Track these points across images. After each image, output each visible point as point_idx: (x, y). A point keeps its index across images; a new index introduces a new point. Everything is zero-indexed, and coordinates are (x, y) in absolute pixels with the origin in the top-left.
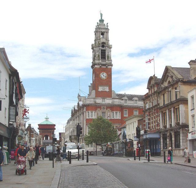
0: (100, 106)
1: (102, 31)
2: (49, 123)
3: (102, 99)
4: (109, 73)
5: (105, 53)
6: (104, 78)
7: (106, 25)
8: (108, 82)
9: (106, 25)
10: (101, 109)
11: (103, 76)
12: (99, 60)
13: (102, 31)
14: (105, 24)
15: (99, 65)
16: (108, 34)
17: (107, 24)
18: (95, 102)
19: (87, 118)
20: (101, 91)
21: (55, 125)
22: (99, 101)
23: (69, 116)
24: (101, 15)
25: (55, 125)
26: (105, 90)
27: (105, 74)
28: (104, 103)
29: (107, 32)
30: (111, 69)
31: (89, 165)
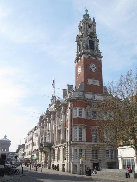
0: (90, 103)
1: (88, 26)
2: (6, 140)
3: (92, 94)
4: (99, 66)
5: (93, 44)
6: (94, 71)
7: (92, 20)
8: (98, 75)
9: (92, 20)
10: (91, 107)
11: (93, 67)
12: (88, 50)
13: (88, 26)
14: (91, 19)
15: (88, 54)
16: (95, 27)
17: (94, 18)
18: (85, 97)
19: (74, 117)
20: (91, 84)
21: (10, 141)
22: (89, 96)
23: (36, 122)
24: (87, 11)
25: (10, 141)
26: (96, 84)
27: (94, 66)
28: (94, 99)
29: (94, 26)
30: (101, 61)
31: (24, 176)
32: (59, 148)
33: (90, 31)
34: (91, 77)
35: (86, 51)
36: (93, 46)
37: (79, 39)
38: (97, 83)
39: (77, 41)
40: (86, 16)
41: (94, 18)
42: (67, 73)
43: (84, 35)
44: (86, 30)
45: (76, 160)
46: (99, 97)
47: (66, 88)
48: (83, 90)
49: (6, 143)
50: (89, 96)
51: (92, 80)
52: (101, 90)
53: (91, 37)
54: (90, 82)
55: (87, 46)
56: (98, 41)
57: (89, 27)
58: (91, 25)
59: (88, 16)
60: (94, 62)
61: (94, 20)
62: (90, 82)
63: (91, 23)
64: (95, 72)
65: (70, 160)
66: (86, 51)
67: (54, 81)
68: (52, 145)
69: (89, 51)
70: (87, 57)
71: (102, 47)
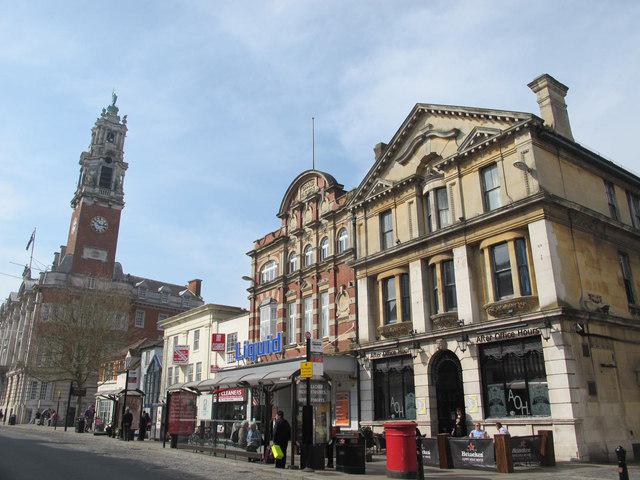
1: (110, 132)
5: (110, 175)
11: (100, 224)
13: (110, 132)
17: (125, 117)
24: (115, 98)
27: (102, 221)
29: (123, 134)
32: (611, 366)
33: (109, 146)
34: (92, 244)
35: (91, 190)
36: (110, 180)
37: (85, 159)
38: (103, 256)
39: (81, 163)
40: (114, 109)
41: (125, 117)
42: (58, 229)
43: (94, 154)
44: (102, 144)
45: (32, 402)
46: (102, 285)
47: (59, 251)
48: (69, 268)
49: (95, 306)
50: (78, 281)
51: (91, 250)
52: (111, 269)
53: (108, 160)
54: (88, 253)
55: (94, 180)
56: (125, 166)
57: (111, 135)
58: (116, 132)
59: (116, 110)
60: (102, 213)
61: (125, 121)
62: (88, 253)
63: (115, 129)
64: (104, 234)
65: (22, 401)
66: (91, 190)
67: (32, 239)
68: (7, 371)
69: (97, 190)
70: (90, 203)
71: (131, 184)
